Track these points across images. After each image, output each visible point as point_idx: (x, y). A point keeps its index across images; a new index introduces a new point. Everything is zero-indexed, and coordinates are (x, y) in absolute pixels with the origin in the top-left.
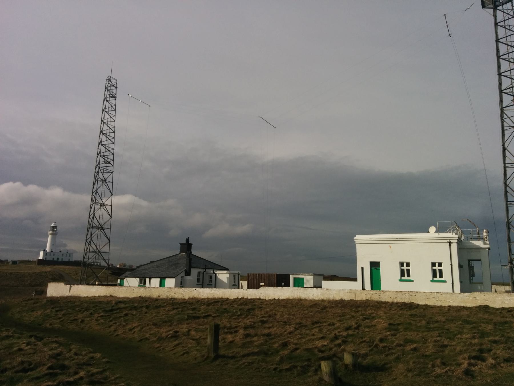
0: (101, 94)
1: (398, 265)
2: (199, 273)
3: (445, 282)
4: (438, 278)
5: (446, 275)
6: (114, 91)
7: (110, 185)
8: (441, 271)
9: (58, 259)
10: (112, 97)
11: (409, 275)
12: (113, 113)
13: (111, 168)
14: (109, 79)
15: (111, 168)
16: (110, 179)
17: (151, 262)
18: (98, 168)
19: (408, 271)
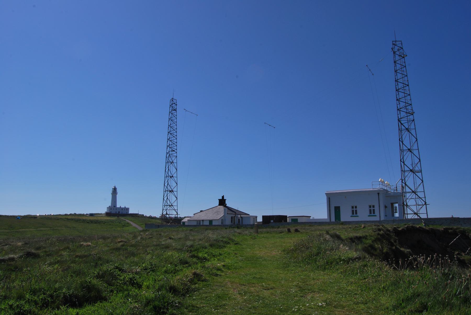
0: (167, 109)
1: (368, 207)
2: (232, 217)
3: (376, 216)
4: (355, 215)
5: (377, 213)
6: (175, 107)
7: (176, 179)
8: (374, 210)
9: (119, 212)
10: (175, 110)
11: (356, 213)
12: (175, 114)
13: (175, 154)
14: (172, 99)
15: (175, 154)
16: (175, 161)
17: (201, 211)
18: (168, 155)
19: (356, 211)
